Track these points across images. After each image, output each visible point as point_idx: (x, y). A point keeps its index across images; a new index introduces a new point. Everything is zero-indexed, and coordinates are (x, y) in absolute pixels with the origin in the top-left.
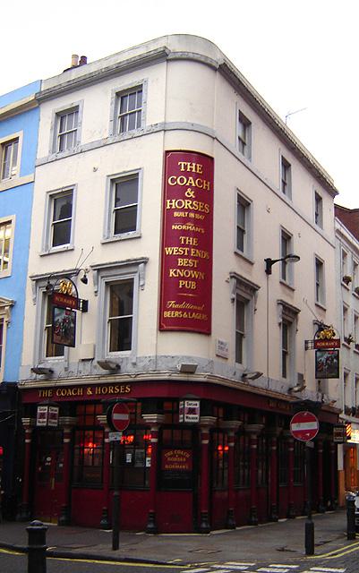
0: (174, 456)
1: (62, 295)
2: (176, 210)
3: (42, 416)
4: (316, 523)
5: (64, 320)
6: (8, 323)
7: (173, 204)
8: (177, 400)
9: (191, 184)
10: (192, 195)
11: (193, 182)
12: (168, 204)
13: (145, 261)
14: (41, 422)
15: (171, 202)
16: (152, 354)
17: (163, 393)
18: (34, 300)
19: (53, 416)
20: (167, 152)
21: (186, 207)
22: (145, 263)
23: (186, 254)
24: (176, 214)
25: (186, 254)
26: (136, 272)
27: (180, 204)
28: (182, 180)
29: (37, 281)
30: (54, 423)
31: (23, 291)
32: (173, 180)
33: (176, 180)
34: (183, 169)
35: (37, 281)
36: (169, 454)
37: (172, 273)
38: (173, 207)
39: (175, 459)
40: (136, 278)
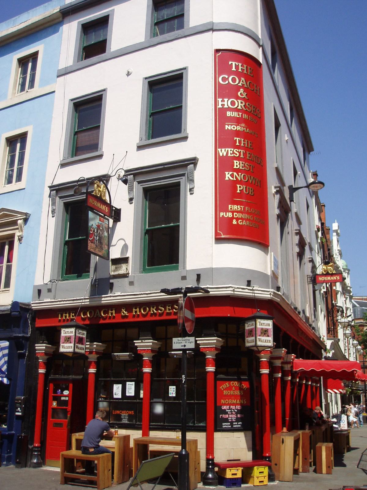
0: (230, 388)
1: (96, 197)
2: (229, 109)
3: (68, 339)
4: (297, 467)
5: (98, 226)
6: (20, 240)
7: (225, 103)
8: (241, 321)
9: (243, 85)
10: (244, 96)
11: (245, 83)
12: (220, 103)
13: (194, 161)
14: (66, 348)
15: (223, 101)
16: (5, 358)
17: (227, 312)
18: (53, 212)
19: (80, 341)
20: (217, 51)
21: (239, 107)
22: (195, 164)
23: (242, 156)
24: (229, 114)
25: (242, 156)
26: (183, 175)
27: (233, 103)
28: (234, 80)
29: (58, 191)
30: (82, 349)
31: (39, 204)
32: (224, 79)
33: (228, 79)
34: (234, 69)
35: (58, 191)
36: (224, 386)
37: (228, 176)
38: (226, 106)
39: (232, 392)
40: (183, 180)
